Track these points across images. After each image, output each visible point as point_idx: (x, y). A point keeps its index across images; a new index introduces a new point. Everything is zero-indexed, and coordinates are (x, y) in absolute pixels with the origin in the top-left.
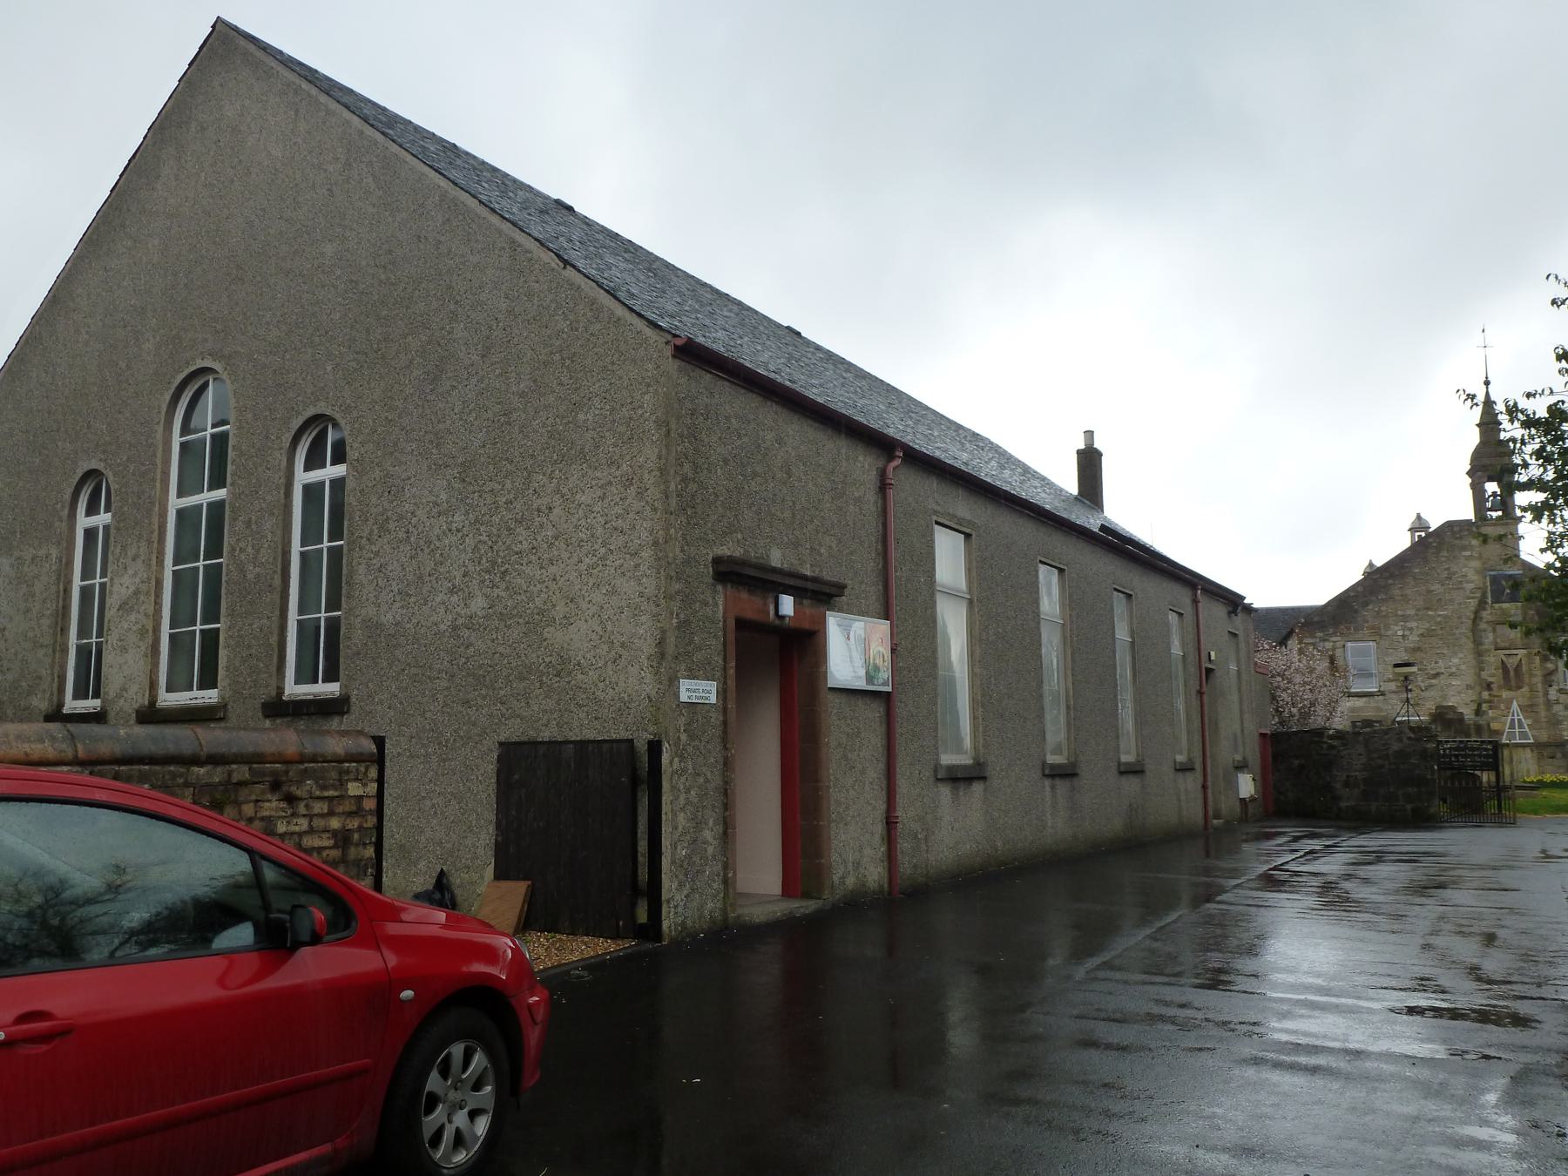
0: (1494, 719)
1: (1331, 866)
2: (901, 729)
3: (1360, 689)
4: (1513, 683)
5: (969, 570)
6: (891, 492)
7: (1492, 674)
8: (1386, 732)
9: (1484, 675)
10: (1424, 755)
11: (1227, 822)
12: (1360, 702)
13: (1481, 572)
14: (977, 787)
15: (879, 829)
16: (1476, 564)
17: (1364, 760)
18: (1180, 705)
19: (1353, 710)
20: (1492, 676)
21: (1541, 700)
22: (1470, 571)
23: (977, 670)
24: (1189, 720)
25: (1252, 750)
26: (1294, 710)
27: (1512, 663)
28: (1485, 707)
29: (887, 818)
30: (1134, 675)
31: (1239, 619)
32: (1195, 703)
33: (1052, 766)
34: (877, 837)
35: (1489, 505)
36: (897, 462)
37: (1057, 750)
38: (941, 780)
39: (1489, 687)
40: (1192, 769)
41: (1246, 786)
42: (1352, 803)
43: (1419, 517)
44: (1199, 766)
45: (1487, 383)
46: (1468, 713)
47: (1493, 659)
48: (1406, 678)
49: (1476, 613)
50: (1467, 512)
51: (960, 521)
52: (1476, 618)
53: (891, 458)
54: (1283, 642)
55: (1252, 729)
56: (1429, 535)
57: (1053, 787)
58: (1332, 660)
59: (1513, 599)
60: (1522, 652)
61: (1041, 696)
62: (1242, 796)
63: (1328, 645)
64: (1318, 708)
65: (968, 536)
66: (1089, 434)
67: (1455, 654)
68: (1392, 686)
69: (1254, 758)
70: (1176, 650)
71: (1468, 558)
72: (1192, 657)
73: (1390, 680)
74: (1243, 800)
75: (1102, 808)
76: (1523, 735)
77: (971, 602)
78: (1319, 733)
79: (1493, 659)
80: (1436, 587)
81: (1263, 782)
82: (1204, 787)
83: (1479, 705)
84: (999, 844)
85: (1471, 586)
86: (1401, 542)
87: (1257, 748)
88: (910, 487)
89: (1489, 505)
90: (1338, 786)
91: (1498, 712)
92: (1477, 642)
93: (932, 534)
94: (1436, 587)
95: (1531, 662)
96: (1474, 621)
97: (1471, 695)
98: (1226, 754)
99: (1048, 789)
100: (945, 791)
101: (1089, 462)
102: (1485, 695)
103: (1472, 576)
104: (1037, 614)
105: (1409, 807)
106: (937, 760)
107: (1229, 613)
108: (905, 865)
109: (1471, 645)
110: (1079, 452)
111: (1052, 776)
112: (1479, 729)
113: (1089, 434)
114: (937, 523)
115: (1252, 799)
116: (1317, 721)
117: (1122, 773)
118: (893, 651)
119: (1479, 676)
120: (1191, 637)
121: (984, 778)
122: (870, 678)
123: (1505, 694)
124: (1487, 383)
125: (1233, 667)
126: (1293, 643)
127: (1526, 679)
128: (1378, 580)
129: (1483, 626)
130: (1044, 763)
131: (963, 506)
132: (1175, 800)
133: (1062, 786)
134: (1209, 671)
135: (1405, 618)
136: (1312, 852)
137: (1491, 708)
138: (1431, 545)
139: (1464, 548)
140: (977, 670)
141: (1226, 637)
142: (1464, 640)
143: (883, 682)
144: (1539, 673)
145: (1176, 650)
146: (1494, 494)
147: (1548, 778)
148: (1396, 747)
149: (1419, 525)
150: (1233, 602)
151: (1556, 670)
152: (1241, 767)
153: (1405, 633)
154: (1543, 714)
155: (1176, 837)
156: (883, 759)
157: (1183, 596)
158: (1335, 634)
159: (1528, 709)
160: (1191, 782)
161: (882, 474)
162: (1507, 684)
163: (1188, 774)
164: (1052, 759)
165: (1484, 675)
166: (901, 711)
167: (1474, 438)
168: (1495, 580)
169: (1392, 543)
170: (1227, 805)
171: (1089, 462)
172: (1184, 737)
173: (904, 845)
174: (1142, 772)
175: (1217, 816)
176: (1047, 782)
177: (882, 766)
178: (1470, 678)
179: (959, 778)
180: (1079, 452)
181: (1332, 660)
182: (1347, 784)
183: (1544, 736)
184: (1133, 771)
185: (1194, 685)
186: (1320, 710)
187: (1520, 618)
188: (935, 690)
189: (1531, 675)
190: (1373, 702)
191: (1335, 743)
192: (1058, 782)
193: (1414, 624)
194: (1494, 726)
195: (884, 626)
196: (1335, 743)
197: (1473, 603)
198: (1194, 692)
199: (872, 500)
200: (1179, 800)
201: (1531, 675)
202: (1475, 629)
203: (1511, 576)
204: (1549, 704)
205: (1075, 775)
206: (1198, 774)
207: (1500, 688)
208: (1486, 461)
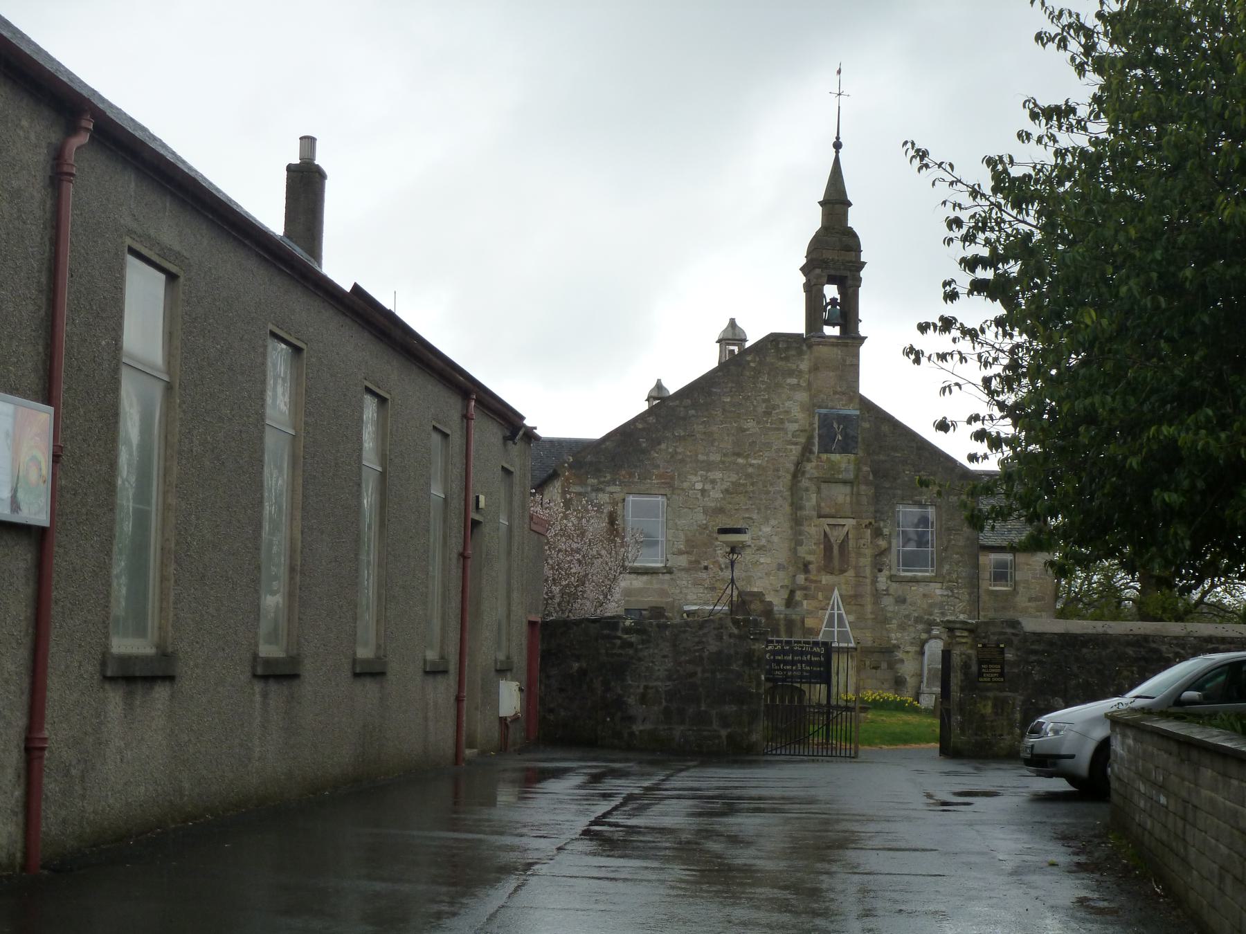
0: (810, 612)
1: (672, 814)
2: (59, 592)
3: (650, 563)
4: (836, 562)
5: (169, 336)
6: (70, 190)
7: (811, 551)
8: (702, 625)
9: (802, 551)
10: (749, 659)
11: (483, 753)
12: (638, 582)
13: (810, 408)
14: (161, 693)
15: (14, 758)
16: (802, 396)
17: (670, 664)
18: (436, 570)
19: (627, 593)
20: (811, 552)
21: (868, 588)
22: (794, 407)
23: (172, 501)
24: (445, 597)
25: (517, 647)
26: (556, 589)
27: (836, 536)
28: (799, 595)
29: (28, 740)
30: (382, 524)
31: (516, 449)
32: (456, 572)
33: (268, 662)
34: (10, 774)
35: (826, 315)
36: (83, 139)
37: (273, 638)
38: (112, 679)
39: (806, 567)
40: (445, 672)
41: (510, 698)
42: (648, 726)
43: (733, 323)
44: (455, 671)
45: (837, 145)
46: (777, 601)
47: (813, 530)
48: (733, 551)
49: (798, 464)
50: (797, 325)
51: (165, 251)
52: (797, 473)
53: (72, 129)
54: (541, 486)
55: (522, 615)
56: (744, 352)
57: (265, 695)
58: (612, 519)
59: (845, 449)
60: (851, 522)
61: (258, 549)
62: (502, 714)
63: (603, 498)
64: (589, 587)
65: (171, 277)
66: (308, 143)
67: (767, 520)
68: (683, 561)
69: (520, 660)
70: (437, 491)
71: (794, 388)
72: (457, 504)
73: (680, 553)
74: (503, 720)
75: (319, 732)
76: (843, 636)
77: (169, 387)
78: (611, 623)
79: (813, 530)
80: (750, 424)
81: (527, 692)
82: (459, 700)
83: (792, 592)
84: (186, 785)
85: (795, 427)
86: (704, 359)
87: (524, 642)
88: (100, 186)
89: (826, 315)
90: (631, 700)
91: (814, 603)
92: (796, 506)
93: (122, 268)
94: (750, 424)
95: (859, 537)
96: (795, 476)
97: (782, 579)
98: (486, 651)
99: (258, 698)
100: (114, 698)
101: (305, 184)
102: (801, 579)
103: (797, 412)
104: (262, 417)
105: (724, 733)
106: (107, 647)
107: (506, 439)
108: (51, 819)
109: (787, 509)
110: (290, 168)
111: (265, 678)
112: (790, 624)
113: (308, 143)
114: (134, 252)
115: (516, 719)
116: (585, 608)
117: (357, 675)
118: (56, 458)
119: (794, 551)
120: (457, 471)
121: (170, 678)
122: (15, 505)
123: (826, 579)
124: (837, 145)
125: (504, 521)
126: (554, 491)
127: (853, 560)
128: (666, 411)
129: (805, 483)
130: (255, 657)
131: (172, 228)
132: (418, 719)
133: (371, 686)
134: (476, 524)
135: (709, 466)
136: (630, 798)
137: (806, 597)
138: (746, 365)
139: (791, 373)
140: (172, 501)
141: (500, 472)
142: (779, 501)
143: (36, 512)
144: (868, 552)
145: (437, 491)
146: (833, 300)
147: (869, 695)
148: (713, 647)
149: (732, 335)
150: (508, 421)
151: (888, 549)
152: (504, 670)
153: (707, 486)
154: (869, 608)
155: (417, 775)
156: (27, 641)
157: (451, 406)
158: (613, 482)
159: (852, 600)
160: (442, 691)
161: (58, 156)
162: (828, 568)
163: (439, 678)
164: (267, 650)
165: (802, 551)
166: (62, 560)
167: (814, 221)
168: (825, 422)
169: (689, 360)
170: (483, 728)
171: (305, 184)
172: (436, 623)
173: (51, 785)
174: (426, 673)
175: (471, 746)
176: (258, 687)
177: (23, 653)
178: (782, 556)
179: (134, 677)
180: (290, 168)
181: (612, 519)
182: (643, 699)
183: (868, 639)
184: (370, 672)
185: (456, 545)
186: (590, 591)
187: (851, 476)
188: (111, 529)
189: (859, 555)
190: (655, 583)
191: (633, 638)
192: (273, 686)
193: (717, 475)
194: (809, 622)
195: (43, 416)
196: (633, 638)
197: (796, 450)
198: (454, 556)
199: (38, 196)
200: (426, 719)
201: (859, 555)
202: (794, 487)
203: (846, 417)
204: (877, 595)
205: (294, 677)
206: (453, 678)
207: (819, 570)
208: (829, 255)
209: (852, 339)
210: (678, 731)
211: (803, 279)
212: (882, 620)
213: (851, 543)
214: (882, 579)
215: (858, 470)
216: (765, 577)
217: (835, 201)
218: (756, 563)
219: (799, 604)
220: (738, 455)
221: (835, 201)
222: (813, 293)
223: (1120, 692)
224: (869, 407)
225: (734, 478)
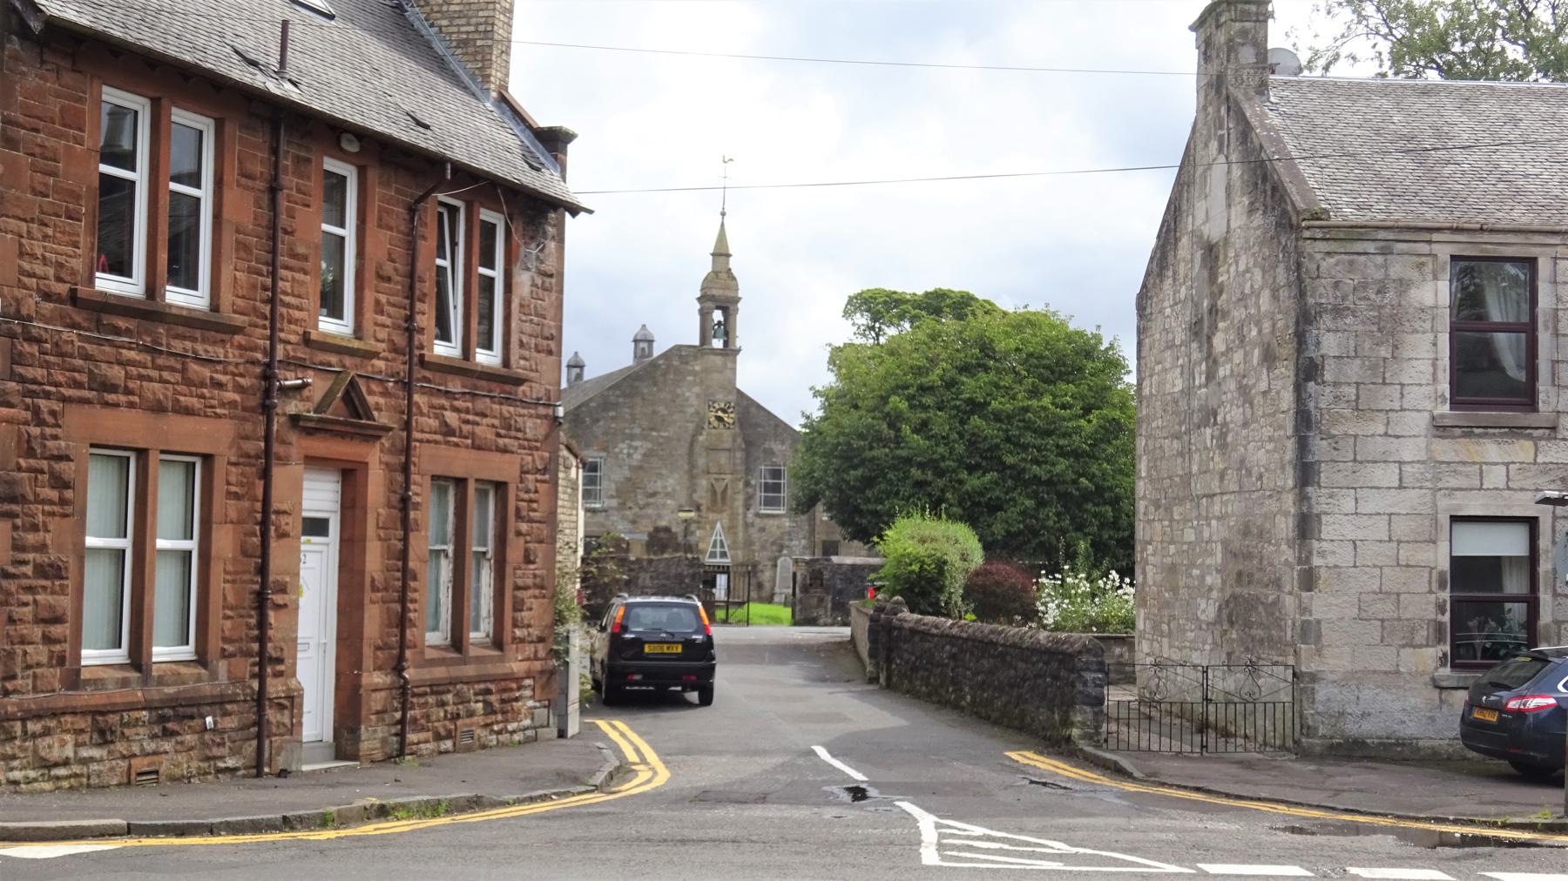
7: (702, 495)
9: (696, 496)
27: (719, 487)
47: (703, 483)
73: (612, 497)
79: (703, 483)
92: (692, 465)
119: (690, 496)
123: (711, 516)
135: (632, 437)
165: (696, 496)
167: (706, 266)
178: (682, 498)
193: (637, 443)
208: (715, 292)
209: (730, 352)
210: (258, 169)
211: (698, 306)
212: (749, 543)
213: (729, 491)
214: (750, 515)
215: (734, 441)
216: (672, 516)
217: (721, 254)
218: (664, 505)
219: (693, 533)
220: (652, 429)
221: (721, 254)
222: (704, 315)
223: (834, 756)
224: (739, 392)
225: (650, 445)
